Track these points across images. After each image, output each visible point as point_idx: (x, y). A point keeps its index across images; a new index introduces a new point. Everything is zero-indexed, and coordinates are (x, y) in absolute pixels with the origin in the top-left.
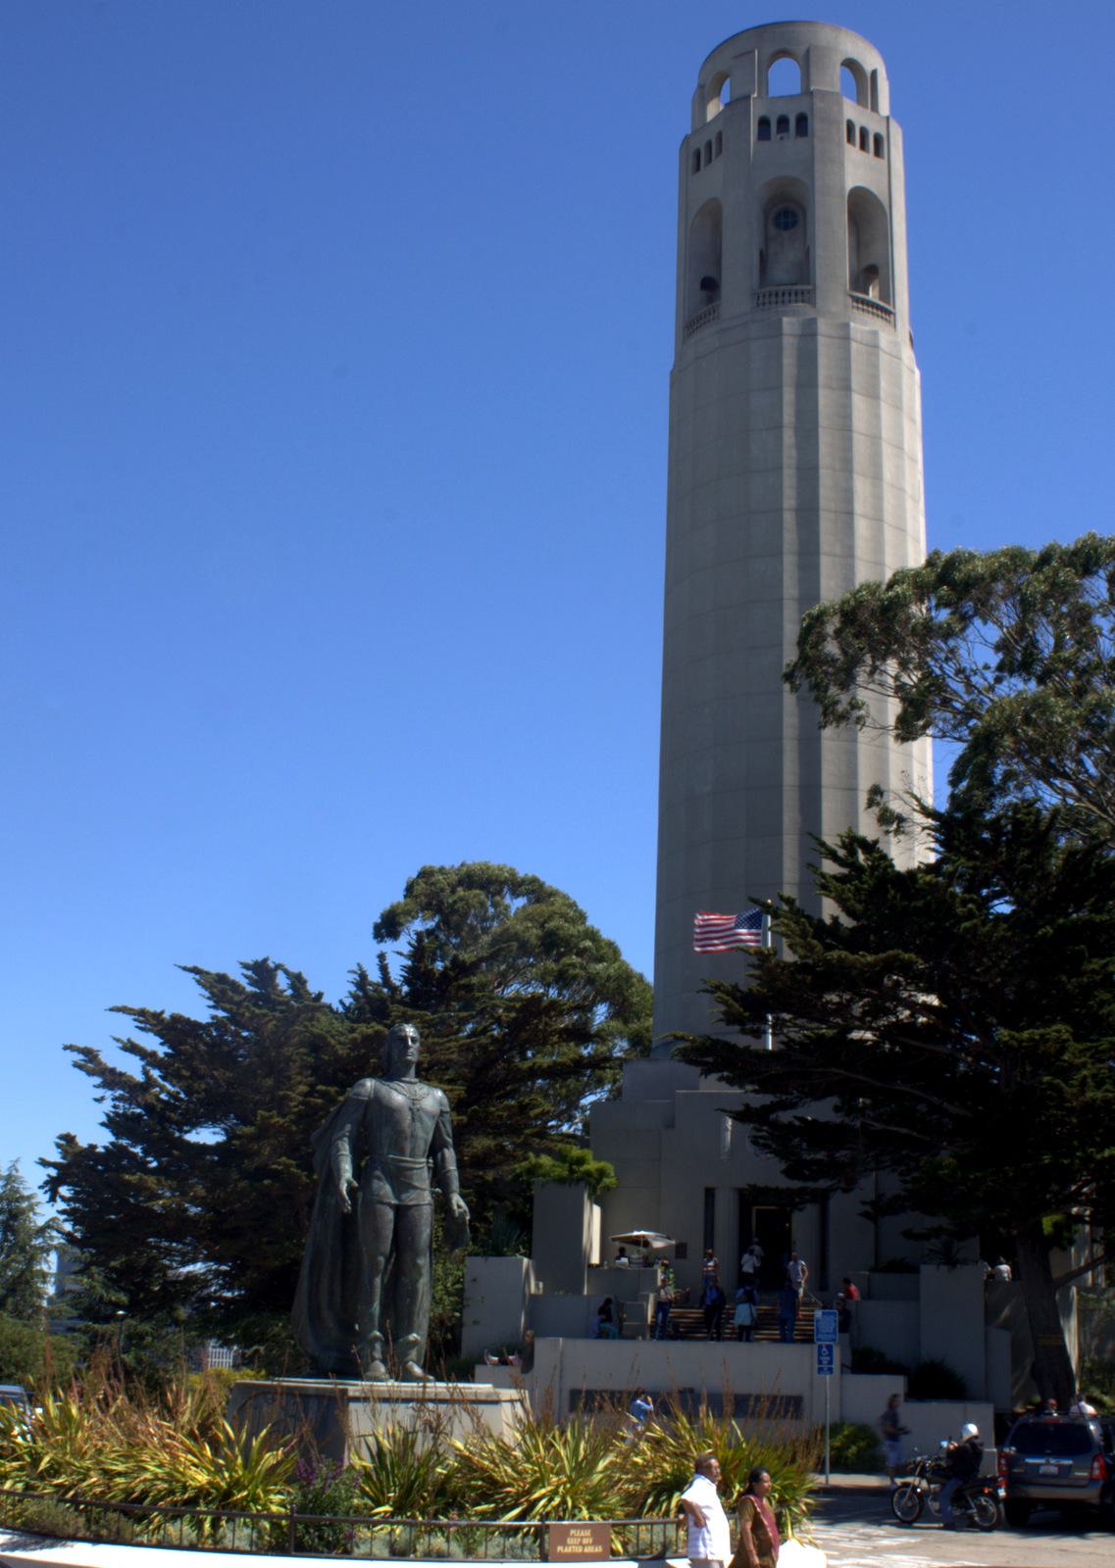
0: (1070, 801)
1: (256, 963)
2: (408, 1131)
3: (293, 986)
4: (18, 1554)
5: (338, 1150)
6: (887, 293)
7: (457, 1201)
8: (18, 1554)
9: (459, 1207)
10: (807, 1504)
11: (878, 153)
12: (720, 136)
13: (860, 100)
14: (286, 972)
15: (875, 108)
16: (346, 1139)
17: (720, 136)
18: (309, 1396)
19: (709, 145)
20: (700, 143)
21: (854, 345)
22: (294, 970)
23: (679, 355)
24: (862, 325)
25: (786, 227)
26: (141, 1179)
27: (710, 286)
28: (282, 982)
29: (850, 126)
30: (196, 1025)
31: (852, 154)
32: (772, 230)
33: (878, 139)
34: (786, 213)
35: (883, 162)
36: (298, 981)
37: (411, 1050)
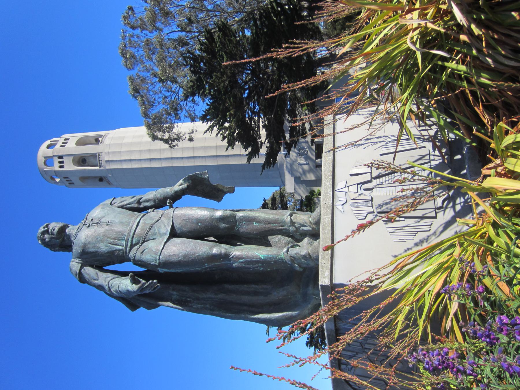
4: (285, 169)
6: (101, 136)
8: (285, 169)
11: (68, 139)
12: (64, 178)
13: (55, 144)
15: (58, 141)
17: (64, 178)
19: (67, 180)
23: (117, 187)
24: (107, 141)
25: (86, 161)
27: (101, 180)
29: (61, 146)
30: (283, 326)
31: (67, 145)
32: (87, 164)
33: (65, 140)
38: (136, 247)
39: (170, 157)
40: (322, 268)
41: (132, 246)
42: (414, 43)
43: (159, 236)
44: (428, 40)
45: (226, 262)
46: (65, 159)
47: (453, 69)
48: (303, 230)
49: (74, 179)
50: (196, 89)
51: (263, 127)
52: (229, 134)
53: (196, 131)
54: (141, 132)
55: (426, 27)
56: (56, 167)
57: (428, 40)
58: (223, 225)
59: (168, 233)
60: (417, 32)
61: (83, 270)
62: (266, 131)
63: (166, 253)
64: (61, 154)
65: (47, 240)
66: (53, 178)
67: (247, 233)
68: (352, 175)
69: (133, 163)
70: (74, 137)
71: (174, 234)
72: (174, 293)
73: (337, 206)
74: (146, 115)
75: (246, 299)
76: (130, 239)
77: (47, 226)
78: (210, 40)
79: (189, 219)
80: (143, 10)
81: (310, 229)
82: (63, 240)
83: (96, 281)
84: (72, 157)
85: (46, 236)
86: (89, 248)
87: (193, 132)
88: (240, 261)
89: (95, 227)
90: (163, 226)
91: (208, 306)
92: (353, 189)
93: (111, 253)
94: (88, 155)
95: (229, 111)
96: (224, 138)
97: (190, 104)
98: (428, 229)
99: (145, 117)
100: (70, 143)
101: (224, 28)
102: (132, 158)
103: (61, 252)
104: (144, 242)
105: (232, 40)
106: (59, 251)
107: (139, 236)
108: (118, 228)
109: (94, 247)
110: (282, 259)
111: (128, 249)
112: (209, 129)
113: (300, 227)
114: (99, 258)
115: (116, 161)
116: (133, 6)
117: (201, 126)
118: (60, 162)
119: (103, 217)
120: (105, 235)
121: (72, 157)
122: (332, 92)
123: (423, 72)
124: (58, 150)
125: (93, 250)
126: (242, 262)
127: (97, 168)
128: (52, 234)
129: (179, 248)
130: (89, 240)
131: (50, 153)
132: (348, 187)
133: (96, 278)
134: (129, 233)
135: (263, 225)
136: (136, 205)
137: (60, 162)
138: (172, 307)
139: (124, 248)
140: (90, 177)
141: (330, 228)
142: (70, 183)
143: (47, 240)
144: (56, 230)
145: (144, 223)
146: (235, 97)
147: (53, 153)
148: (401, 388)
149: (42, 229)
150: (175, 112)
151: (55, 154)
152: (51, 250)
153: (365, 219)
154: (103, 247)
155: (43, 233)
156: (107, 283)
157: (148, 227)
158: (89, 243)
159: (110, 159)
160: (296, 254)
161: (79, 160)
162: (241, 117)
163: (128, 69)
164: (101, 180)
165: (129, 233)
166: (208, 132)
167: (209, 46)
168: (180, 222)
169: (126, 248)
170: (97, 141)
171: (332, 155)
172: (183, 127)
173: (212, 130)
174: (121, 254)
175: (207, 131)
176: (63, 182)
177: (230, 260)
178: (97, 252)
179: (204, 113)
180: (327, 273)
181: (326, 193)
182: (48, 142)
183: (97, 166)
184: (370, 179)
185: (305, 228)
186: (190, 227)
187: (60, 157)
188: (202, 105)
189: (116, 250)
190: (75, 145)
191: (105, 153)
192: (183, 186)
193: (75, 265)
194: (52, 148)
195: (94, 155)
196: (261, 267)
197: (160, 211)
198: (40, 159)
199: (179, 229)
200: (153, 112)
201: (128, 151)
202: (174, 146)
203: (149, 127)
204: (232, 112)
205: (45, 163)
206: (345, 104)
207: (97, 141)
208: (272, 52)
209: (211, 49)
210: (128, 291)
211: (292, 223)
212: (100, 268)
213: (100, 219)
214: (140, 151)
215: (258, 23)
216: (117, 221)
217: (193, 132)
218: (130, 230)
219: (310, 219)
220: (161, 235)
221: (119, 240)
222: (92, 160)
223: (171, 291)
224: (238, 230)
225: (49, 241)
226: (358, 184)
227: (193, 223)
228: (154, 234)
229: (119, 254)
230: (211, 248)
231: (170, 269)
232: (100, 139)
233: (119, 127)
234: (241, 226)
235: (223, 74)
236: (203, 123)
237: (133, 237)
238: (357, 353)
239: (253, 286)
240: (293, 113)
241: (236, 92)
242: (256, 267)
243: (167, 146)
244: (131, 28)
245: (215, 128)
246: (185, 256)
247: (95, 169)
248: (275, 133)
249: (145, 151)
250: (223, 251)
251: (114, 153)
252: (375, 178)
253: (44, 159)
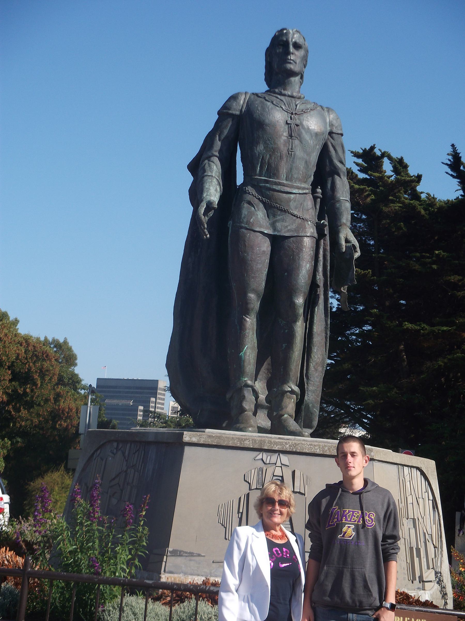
1: (365, 151)
2: (284, 149)
3: (395, 170)
5: (204, 171)
7: (346, 234)
9: (347, 241)
10: (59, 523)
14: (390, 158)
16: (216, 160)
18: (149, 443)
22: (395, 155)
28: (387, 167)
36: (400, 165)
37: (292, 57)
40: (199, 435)
68: (294, 473)
73: (261, 454)
92: (278, 472)
98: (227, 537)
106: (266, 60)
119: (301, 142)
132: (281, 467)
134: (276, 184)
148: (460, 509)
153: (245, 480)
160: (244, 396)
180: (194, 440)
192: (343, 243)
218: (284, 185)
219: (286, 416)
226: (282, 477)
228: (274, 216)
238: (127, 461)
250: (251, 306)
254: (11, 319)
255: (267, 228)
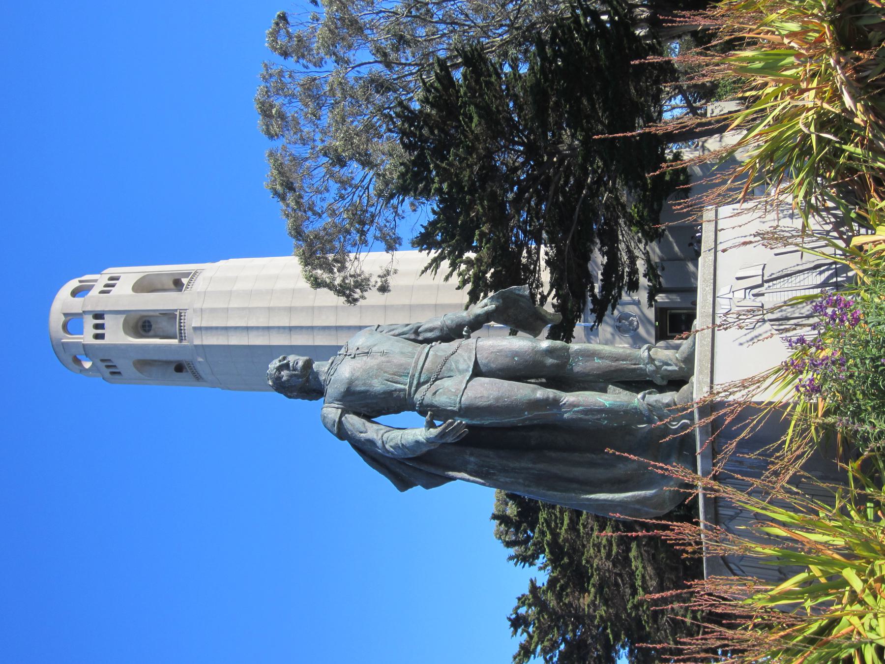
0: (681, 574)
1: (512, 626)
6: (187, 275)
11: (117, 279)
12: (102, 360)
13: (90, 288)
15: (96, 281)
17: (102, 360)
19: (108, 367)
20: (107, 372)
21: (209, 289)
22: (515, 603)
24: (199, 285)
25: (150, 326)
26: (594, 585)
27: (179, 368)
32: (151, 333)
33: (111, 279)
34: (143, 326)
35: (123, 277)
38: (425, 386)
39: (334, 324)
41: (419, 385)
42: (807, 125)
43: (457, 373)
44: (824, 122)
45: (555, 411)
46: (108, 321)
47: (851, 153)
48: (666, 370)
49: (125, 365)
50: (413, 182)
51: (548, 262)
52: (475, 274)
53: (395, 272)
54: (287, 269)
55: (822, 108)
56: (87, 337)
57: (824, 122)
58: (550, 361)
59: (471, 370)
60: (812, 112)
61: (343, 419)
62: (552, 273)
63: (470, 395)
64: (99, 308)
65: (284, 378)
66: (77, 361)
67: (584, 373)
68: (738, 279)
69: (252, 334)
70: (129, 275)
71: (477, 372)
72: (472, 459)
74: (298, 233)
75: (578, 472)
76: (417, 375)
77: (284, 359)
78: (445, 82)
79: (500, 351)
80: (312, 20)
81: (677, 368)
82: (308, 380)
83: (362, 435)
84: (124, 316)
85: (282, 373)
86: (357, 386)
87: (388, 273)
88: (576, 409)
89: (365, 358)
90: (461, 360)
91: (521, 481)
92: (740, 294)
93: (389, 394)
94: (157, 314)
95: (478, 227)
96: (464, 282)
97: (388, 214)
99: (295, 237)
100: (121, 288)
101: (474, 59)
102: (251, 324)
103: (300, 400)
104: (437, 379)
105: (492, 83)
106: (296, 397)
107: (430, 372)
108: (398, 359)
109: (364, 384)
110: (636, 408)
111: (413, 389)
112: (430, 265)
113: (662, 366)
114: (369, 401)
115: (217, 328)
116: (289, 12)
117: (412, 260)
118: (97, 326)
119: (375, 345)
120: (380, 368)
121: (124, 316)
122: (716, 175)
123: (818, 154)
124: (94, 300)
125: (363, 388)
126: (578, 412)
127: (175, 341)
128: (295, 369)
129: (487, 390)
130: (358, 374)
131: (77, 305)
133: (363, 429)
134: (416, 367)
135: (607, 363)
136: (413, 337)
137: (97, 326)
138: (468, 480)
139: (407, 387)
140: (155, 361)
141: (710, 340)
142: (113, 373)
143: (284, 378)
144: (300, 364)
145: (436, 355)
146: (493, 197)
147: (84, 305)
149: (276, 363)
150: (360, 227)
151: (89, 308)
152: (286, 395)
154: (378, 385)
155: (280, 369)
156: (380, 436)
157: (441, 360)
158: (357, 379)
159: (204, 324)
160: (656, 401)
161: (137, 323)
162: (503, 240)
163: (271, 137)
164: (179, 368)
165: (416, 367)
166: (429, 271)
167: (443, 95)
168: (486, 355)
169: (410, 387)
170: (178, 284)
171: (713, 254)
172: (370, 262)
173: (437, 267)
174: (402, 396)
175: (426, 269)
176: (99, 370)
177: (560, 407)
178: (367, 391)
179: (423, 231)
181: (705, 300)
182: (74, 283)
183: (175, 338)
184: (760, 282)
185: (670, 368)
186: (502, 361)
187: (98, 316)
188: (420, 214)
189: (395, 390)
190: (131, 292)
191: (195, 310)
193: (332, 412)
194: (83, 296)
195: (170, 315)
196: (605, 418)
197: (455, 344)
198: (56, 319)
199: (486, 365)
200: (314, 226)
201: (243, 309)
202: (356, 300)
203: (308, 260)
204: (485, 228)
205: (65, 327)
206: (748, 122)
207: (178, 284)
208: (650, 127)
209: (445, 101)
210: (417, 442)
211: (651, 360)
212: (368, 417)
213: (370, 348)
214: (270, 309)
215: (548, 50)
216: (397, 350)
217: (388, 273)
218: (417, 363)
220: (461, 372)
221: (401, 376)
222: (164, 325)
223: (467, 457)
224: (572, 369)
225: (288, 380)
226: (746, 289)
227: (507, 356)
228: (450, 370)
229: (399, 396)
230: (534, 391)
231: (472, 419)
232: (185, 281)
233: (227, 258)
234: (576, 363)
235: (470, 150)
236: (421, 251)
237: (421, 373)
239: (588, 455)
240: (610, 241)
241: (493, 187)
242: (597, 419)
243: (343, 299)
244: (281, 54)
245: (445, 264)
246: (497, 399)
247: (170, 346)
248: (571, 276)
249: (280, 309)
250: (551, 396)
251: (213, 310)
252: (768, 281)
253: (63, 318)
254: (527, 592)
255: (464, 377)
